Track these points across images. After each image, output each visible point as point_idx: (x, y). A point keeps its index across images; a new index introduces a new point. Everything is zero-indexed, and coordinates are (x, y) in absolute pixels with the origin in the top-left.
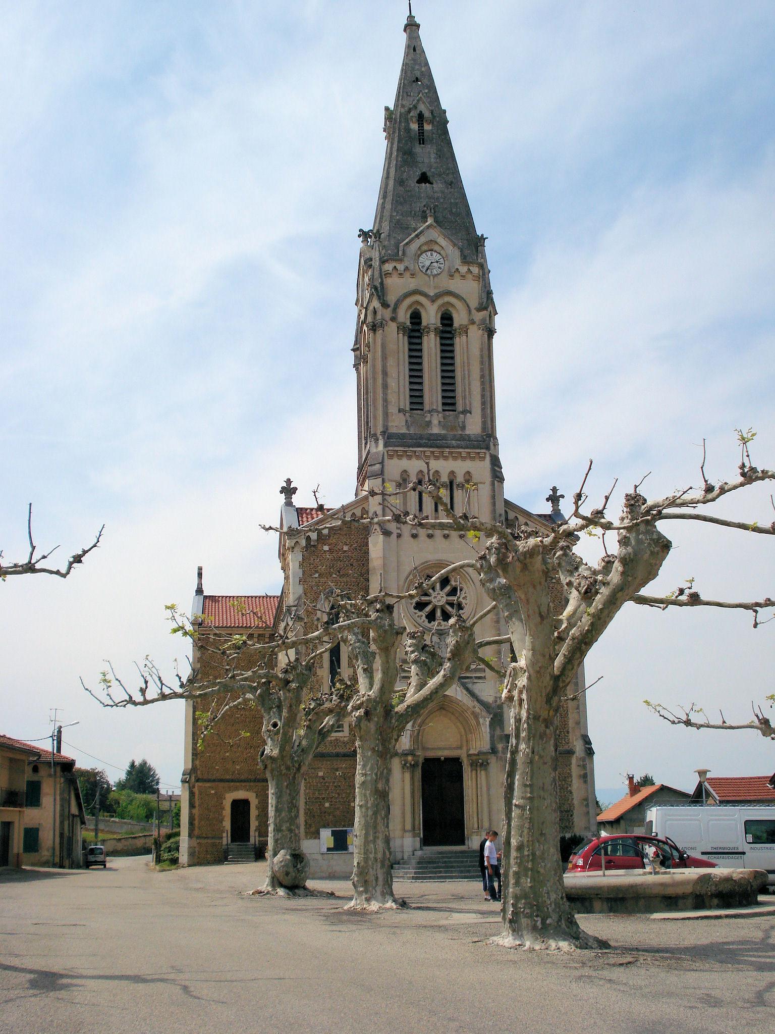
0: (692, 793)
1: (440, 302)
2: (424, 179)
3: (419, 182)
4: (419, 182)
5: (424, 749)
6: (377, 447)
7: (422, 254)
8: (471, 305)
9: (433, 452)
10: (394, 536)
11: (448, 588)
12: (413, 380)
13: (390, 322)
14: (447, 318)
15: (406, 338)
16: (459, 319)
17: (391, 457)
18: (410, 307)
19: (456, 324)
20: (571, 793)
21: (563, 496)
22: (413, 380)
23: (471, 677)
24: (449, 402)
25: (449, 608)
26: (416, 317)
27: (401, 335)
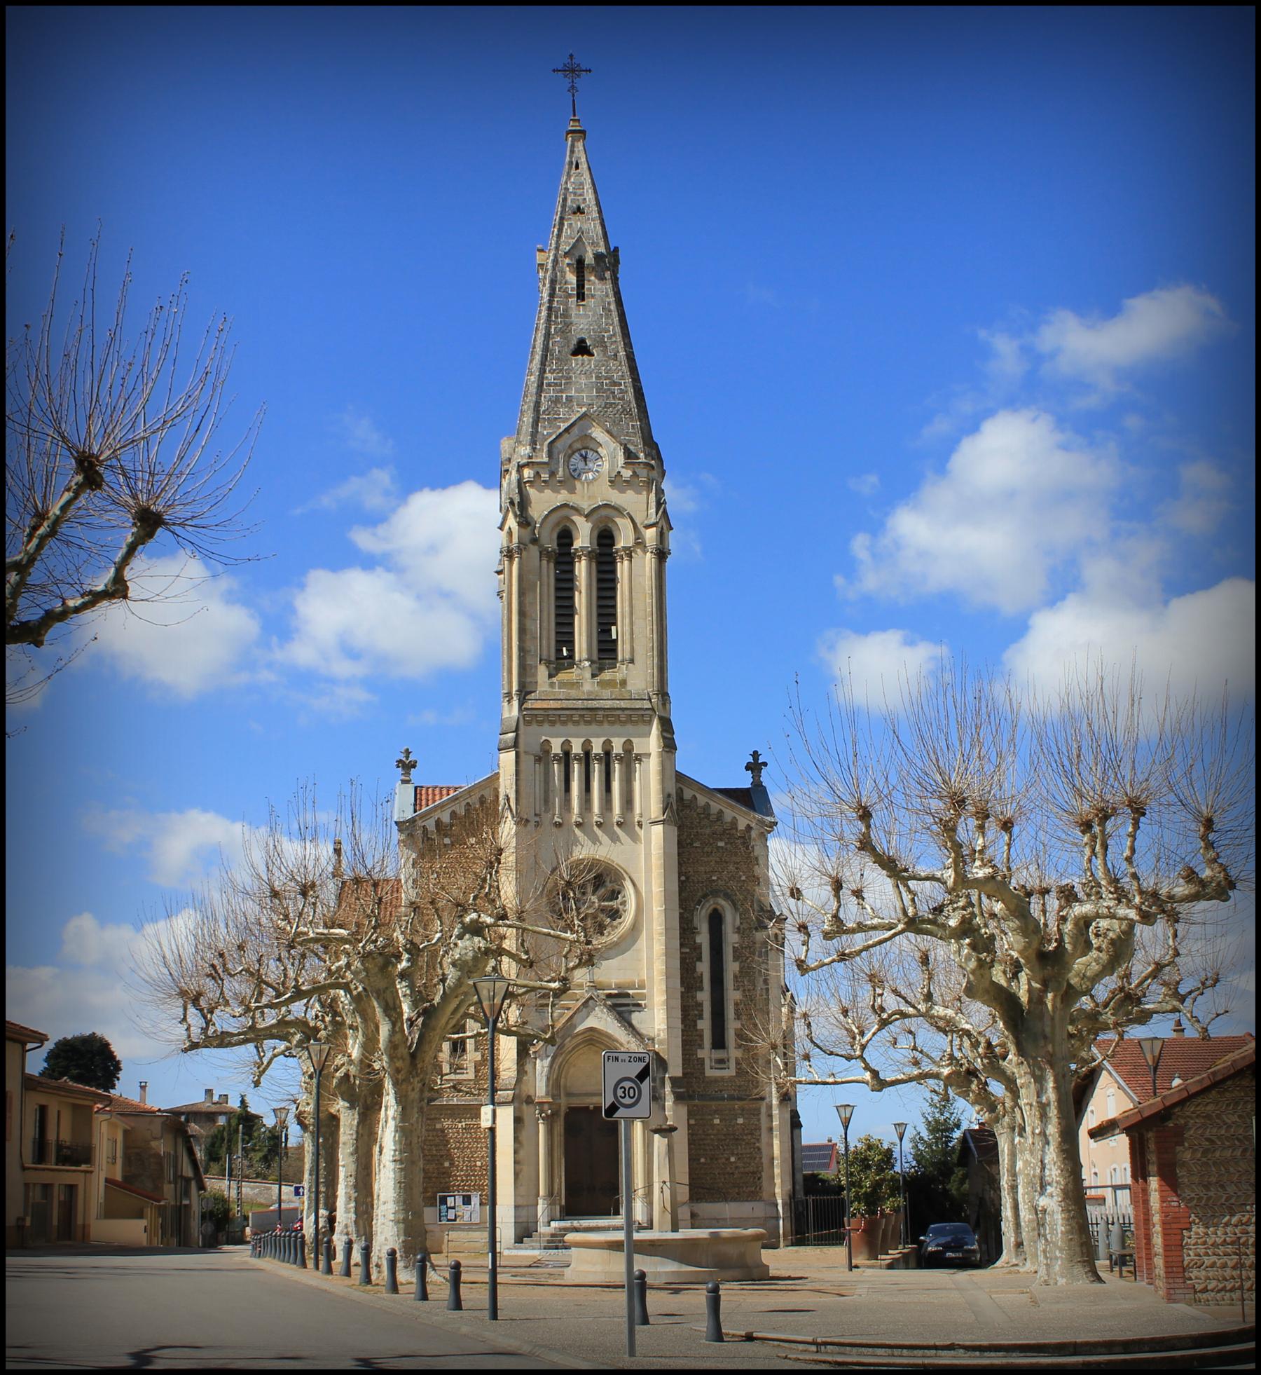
0: (27, 1071)
1: (595, 516)
2: (582, 349)
3: (582, 341)
4: (575, 353)
5: (569, 1095)
6: (510, 711)
7: (573, 453)
8: (637, 521)
9: (582, 716)
10: (532, 824)
11: (602, 891)
12: (603, 576)
13: (531, 546)
14: (605, 538)
15: (552, 565)
16: (624, 538)
17: (528, 723)
18: (558, 524)
19: (620, 544)
20: (759, 1149)
21: (765, 764)
22: (603, 576)
23: (628, 1005)
24: (606, 650)
25: (601, 916)
26: (566, 537)
27: (544, 562)
